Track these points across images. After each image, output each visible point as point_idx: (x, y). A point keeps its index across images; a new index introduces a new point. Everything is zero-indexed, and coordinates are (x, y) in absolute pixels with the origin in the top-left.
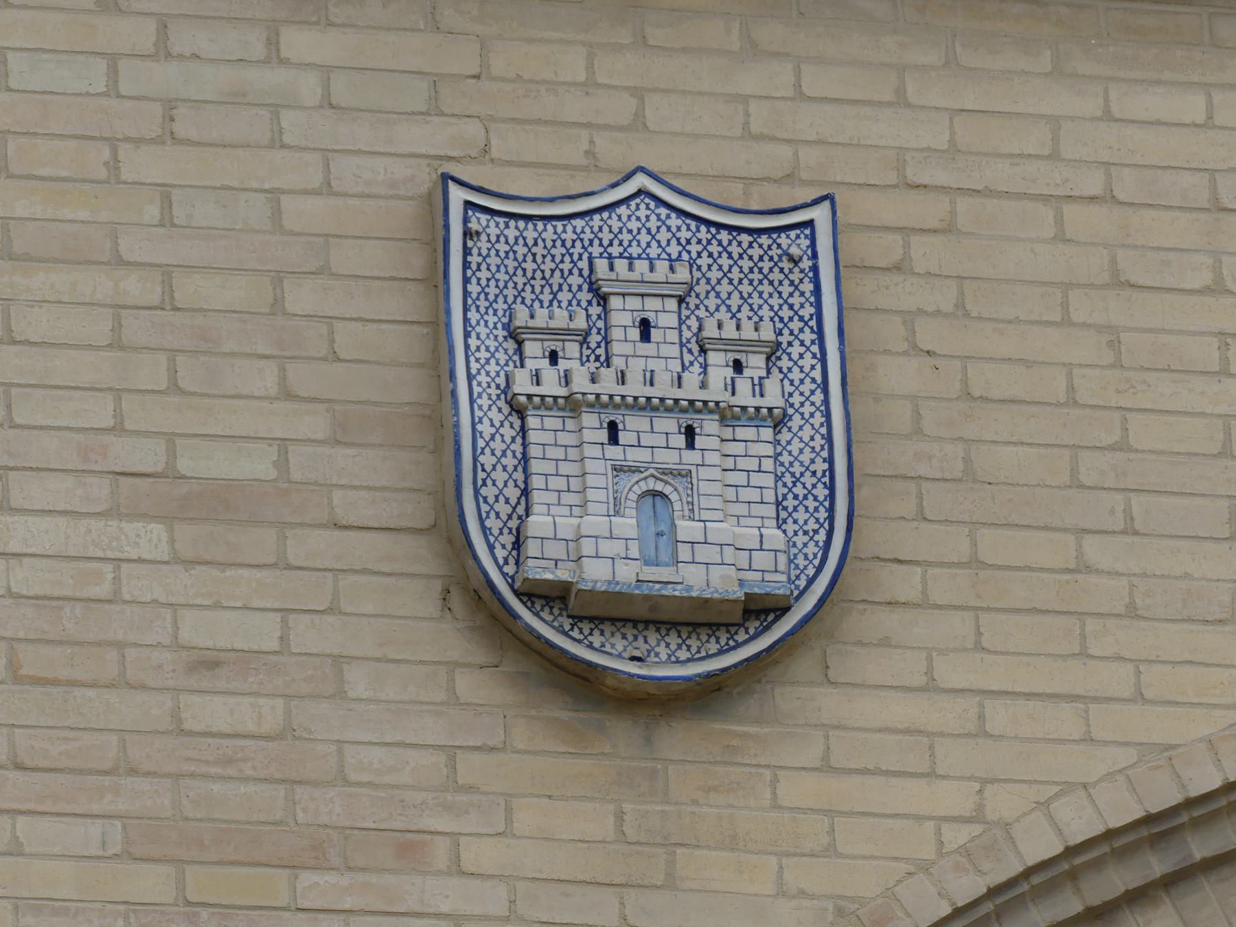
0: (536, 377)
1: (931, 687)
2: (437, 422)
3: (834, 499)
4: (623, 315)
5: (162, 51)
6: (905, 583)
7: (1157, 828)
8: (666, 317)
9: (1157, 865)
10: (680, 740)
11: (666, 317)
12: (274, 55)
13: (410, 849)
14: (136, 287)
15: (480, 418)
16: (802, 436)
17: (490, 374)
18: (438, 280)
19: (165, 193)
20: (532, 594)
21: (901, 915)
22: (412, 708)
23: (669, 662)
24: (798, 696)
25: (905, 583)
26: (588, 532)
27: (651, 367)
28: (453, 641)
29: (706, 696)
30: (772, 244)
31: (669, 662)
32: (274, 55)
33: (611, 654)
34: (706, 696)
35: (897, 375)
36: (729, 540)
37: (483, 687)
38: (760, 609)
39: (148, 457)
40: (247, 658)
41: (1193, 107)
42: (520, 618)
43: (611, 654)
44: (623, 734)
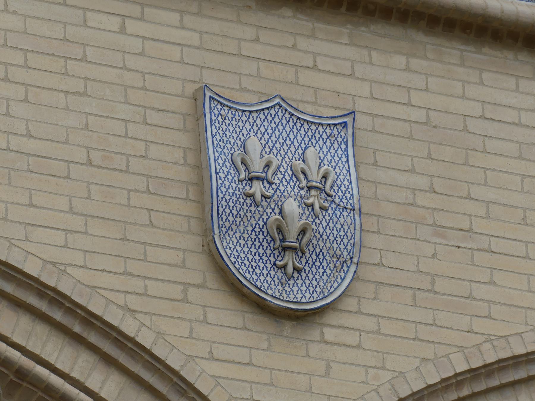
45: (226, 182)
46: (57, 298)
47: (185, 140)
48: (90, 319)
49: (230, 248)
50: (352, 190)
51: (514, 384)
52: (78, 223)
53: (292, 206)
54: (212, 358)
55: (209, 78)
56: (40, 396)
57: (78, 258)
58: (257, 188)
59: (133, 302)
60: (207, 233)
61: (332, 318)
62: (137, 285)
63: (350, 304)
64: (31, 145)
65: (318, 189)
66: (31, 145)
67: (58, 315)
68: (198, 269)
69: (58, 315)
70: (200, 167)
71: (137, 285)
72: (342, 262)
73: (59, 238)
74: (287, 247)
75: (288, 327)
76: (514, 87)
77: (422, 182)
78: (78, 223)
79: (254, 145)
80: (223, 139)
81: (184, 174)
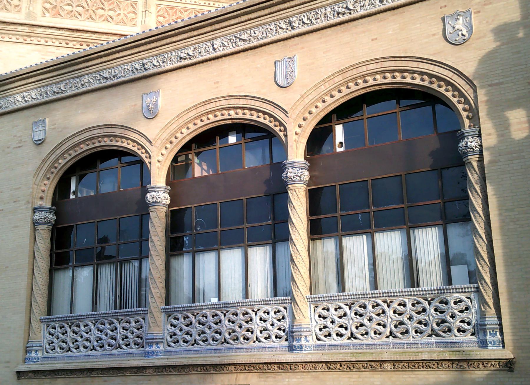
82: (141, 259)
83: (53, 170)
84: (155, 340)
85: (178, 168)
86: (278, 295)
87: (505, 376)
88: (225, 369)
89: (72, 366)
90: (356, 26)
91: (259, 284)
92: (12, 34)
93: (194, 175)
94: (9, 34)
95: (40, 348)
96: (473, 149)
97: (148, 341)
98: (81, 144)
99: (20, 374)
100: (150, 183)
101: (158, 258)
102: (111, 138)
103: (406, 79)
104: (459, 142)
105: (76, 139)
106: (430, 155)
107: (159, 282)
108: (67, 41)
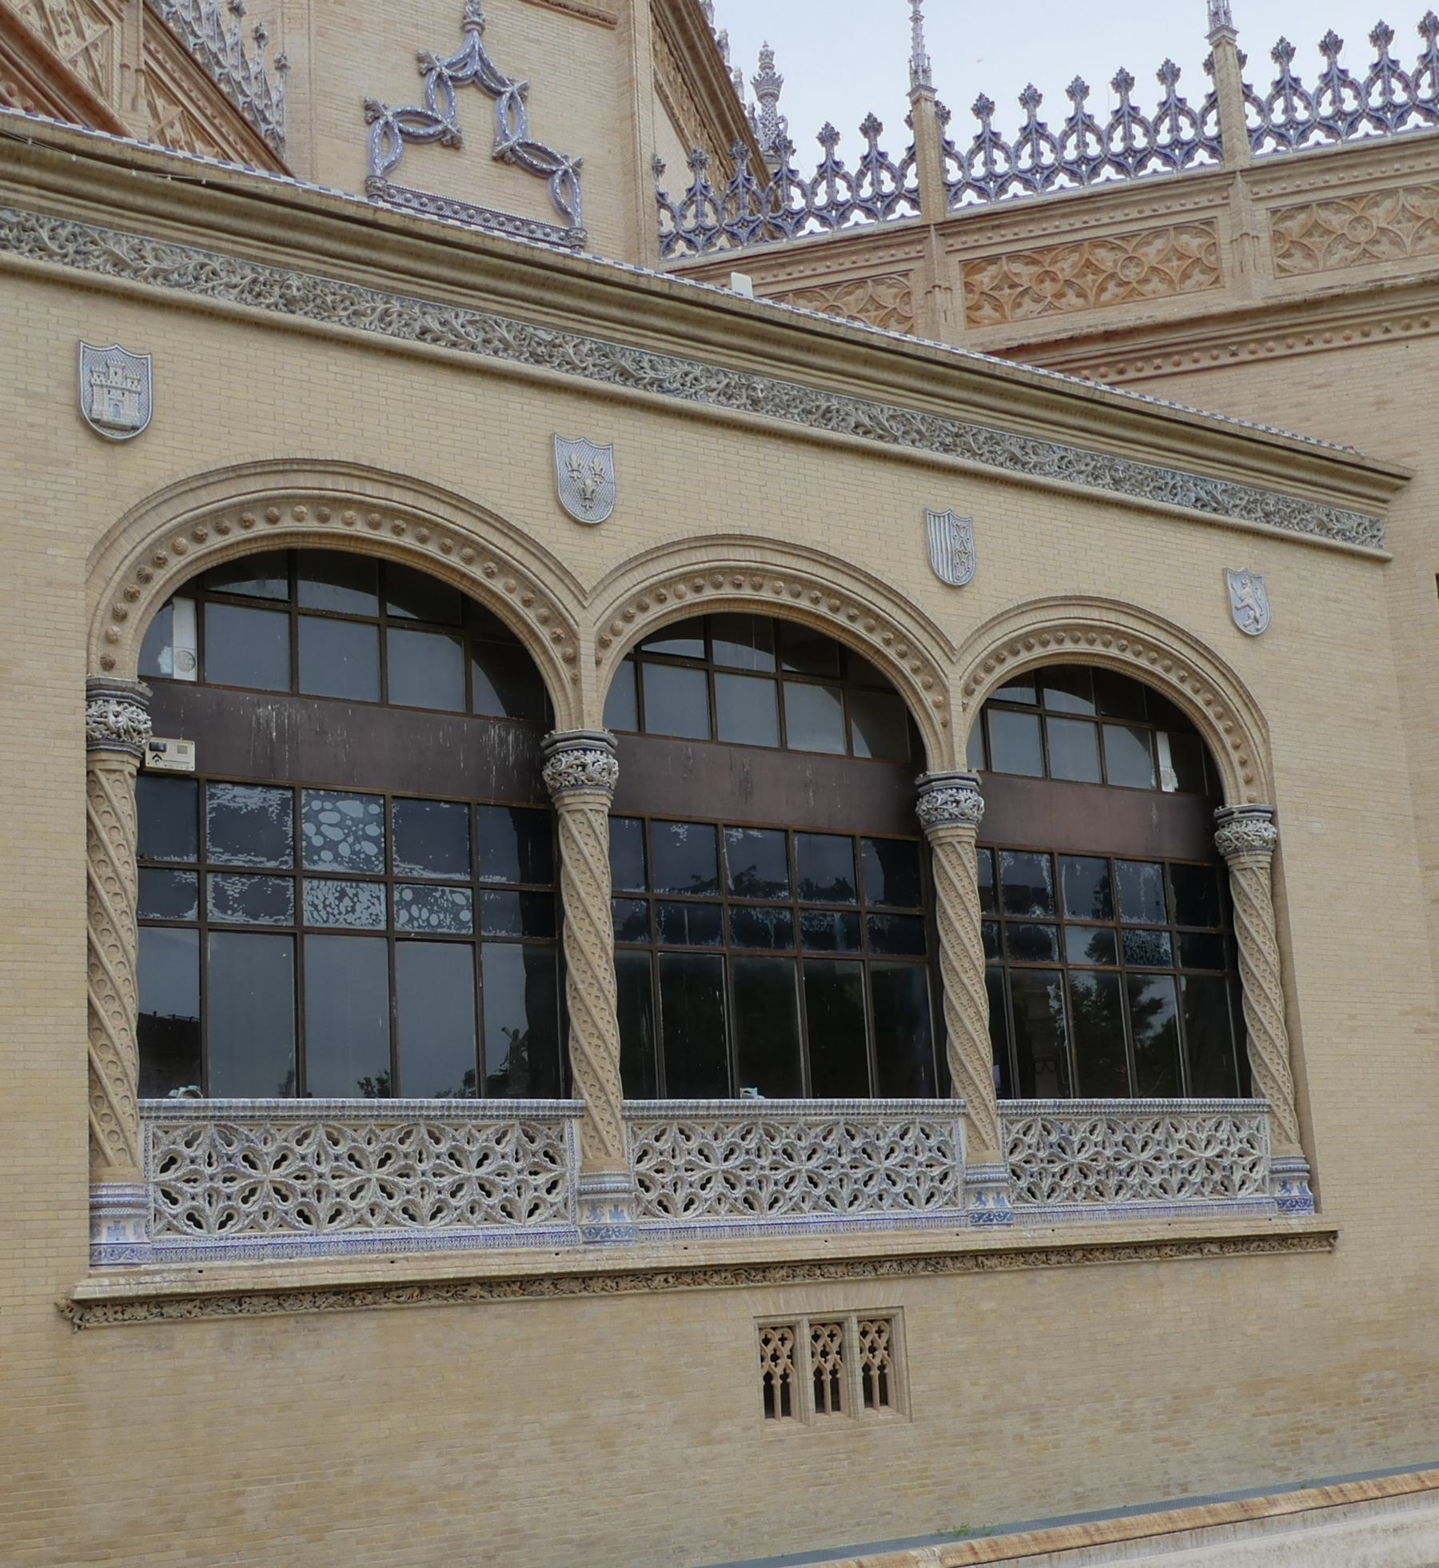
0: (95, 380)
1: (164, 445)
2: (76, 386)
3: (149, 408)
4: (112, 370)
5: (27, 309)
6: (160, 426)
7: (203, 476)
8: (120, 372)
9: (203, 482)
10: (118, 449)
11: (120, 372)
12: (48, 312)
13: (68, 464)
14: (20, 353)
15: (84, 386)
16: (143, 397)
17: (87, 378)
18: (77, 360)
19: (27, 336)
20: (93, 420)
21: (1056, 957)
22: (70, 439)
23: (118, 436)
24: (139, 443)
25: (160, 426)
26: (103, 409)
27: (117, 380)
28: (77, 426)
29: (124, 442)
30: (139, 360)
31: (118, 436)
32: (48, 312)
33: (107, 433)
34: (124, 442)
35: (162, 388)
36: (129, 415)
37: (82, 435)
38: (134, 428)
39: (22, 386)
40: (40, 425)
41: (217, 345)
42: (993, 984)
43: (107, 433)
44: (108, 448)
45: (562, 471)
46: (497, 518)
47: (547, 454)
48: (510, 527)
49: (565, 499)
50: (611, 475)
51: (475, 516)
52: (505, 488)
53: (589, 482)
54: (557, 542)
55: (556, 429)
56: (667, 940)
57: (505, 502)
58: (575, 474)
59: (527, 520)
60: (555, 492)
61: (604, 526)
62: (528, 513)
63: (610, 521)
64: (486, 456)
65: (599, 475)
66: (486, 456)
67: (498, 525)
68: (552, 507)
69: (498, 525)
70: (553, 466)
71: (528, 513)
72: (608, 504)
73: (498, 494)
74: (586, 497)
75: (587, 530)
76: (283, 594)
77: (638, 472)
78: (505, 488)
79: (574, 457)
80: (561, 453)
81: (546, 468)
82: (473, 943)
83: (183, 541)
84: (990, 1185)
85: (633, 729)
86: (314, 1074)
87: (245, 6)
88: (818, 1272)
89: (698, 1257)
90: (577, 404)
91: (177, 859)
92: (1216, 347)
93: (839, 756)
94: (1345, 327)
95: (626, 1195)
96: (119, 736)
97: (584, 1197)
98: (301, 503)
99: (80, 1311)
100: (1223, 804)
101: (122, 1090)
102: (398, 522)
103: (279, 525)
104: (1217, 807)
105: (441, 512)
106: (1392, 32)
107: (109, 1077)
108: (1407, 321)
